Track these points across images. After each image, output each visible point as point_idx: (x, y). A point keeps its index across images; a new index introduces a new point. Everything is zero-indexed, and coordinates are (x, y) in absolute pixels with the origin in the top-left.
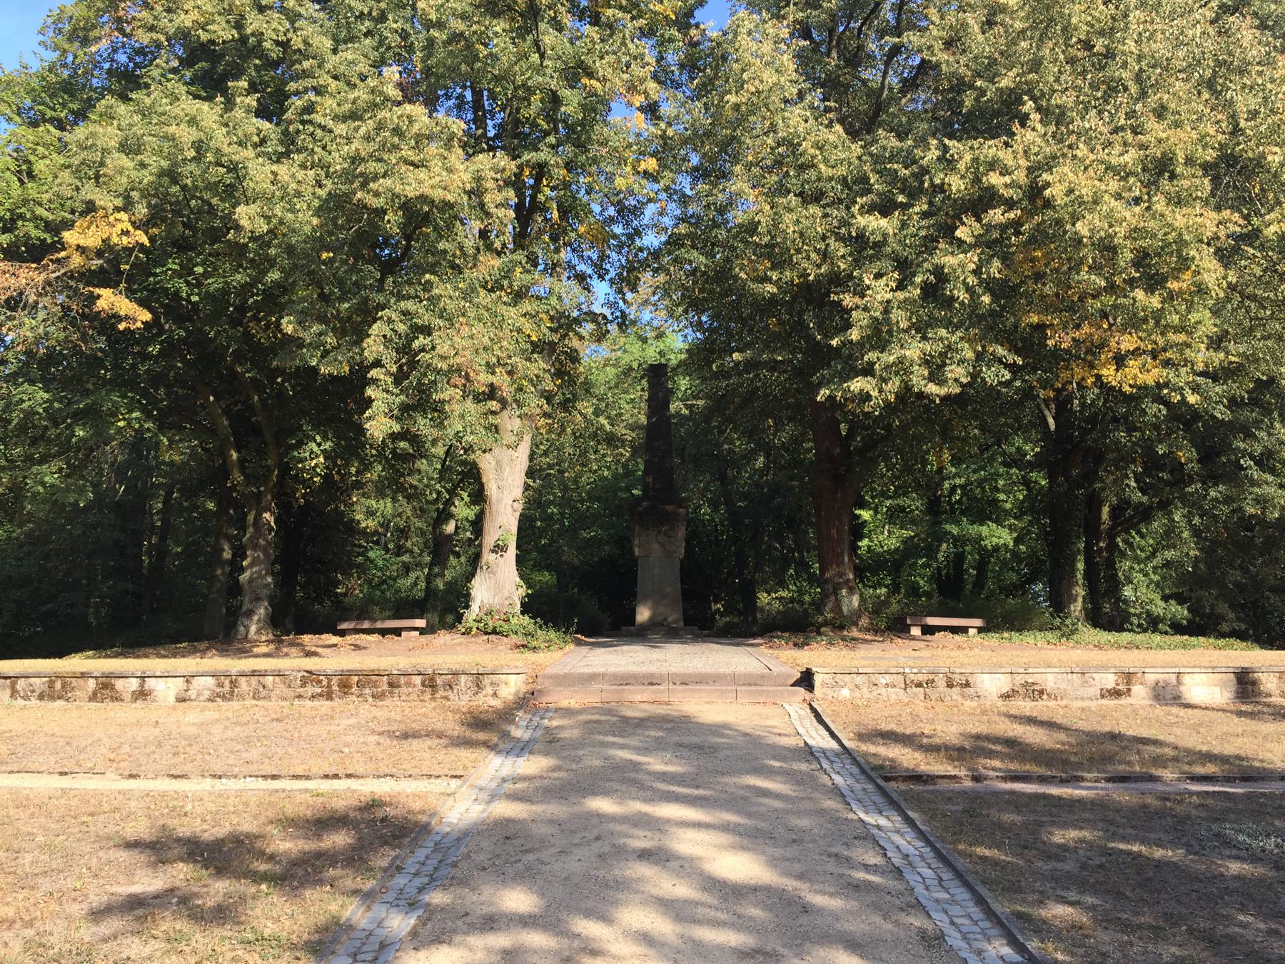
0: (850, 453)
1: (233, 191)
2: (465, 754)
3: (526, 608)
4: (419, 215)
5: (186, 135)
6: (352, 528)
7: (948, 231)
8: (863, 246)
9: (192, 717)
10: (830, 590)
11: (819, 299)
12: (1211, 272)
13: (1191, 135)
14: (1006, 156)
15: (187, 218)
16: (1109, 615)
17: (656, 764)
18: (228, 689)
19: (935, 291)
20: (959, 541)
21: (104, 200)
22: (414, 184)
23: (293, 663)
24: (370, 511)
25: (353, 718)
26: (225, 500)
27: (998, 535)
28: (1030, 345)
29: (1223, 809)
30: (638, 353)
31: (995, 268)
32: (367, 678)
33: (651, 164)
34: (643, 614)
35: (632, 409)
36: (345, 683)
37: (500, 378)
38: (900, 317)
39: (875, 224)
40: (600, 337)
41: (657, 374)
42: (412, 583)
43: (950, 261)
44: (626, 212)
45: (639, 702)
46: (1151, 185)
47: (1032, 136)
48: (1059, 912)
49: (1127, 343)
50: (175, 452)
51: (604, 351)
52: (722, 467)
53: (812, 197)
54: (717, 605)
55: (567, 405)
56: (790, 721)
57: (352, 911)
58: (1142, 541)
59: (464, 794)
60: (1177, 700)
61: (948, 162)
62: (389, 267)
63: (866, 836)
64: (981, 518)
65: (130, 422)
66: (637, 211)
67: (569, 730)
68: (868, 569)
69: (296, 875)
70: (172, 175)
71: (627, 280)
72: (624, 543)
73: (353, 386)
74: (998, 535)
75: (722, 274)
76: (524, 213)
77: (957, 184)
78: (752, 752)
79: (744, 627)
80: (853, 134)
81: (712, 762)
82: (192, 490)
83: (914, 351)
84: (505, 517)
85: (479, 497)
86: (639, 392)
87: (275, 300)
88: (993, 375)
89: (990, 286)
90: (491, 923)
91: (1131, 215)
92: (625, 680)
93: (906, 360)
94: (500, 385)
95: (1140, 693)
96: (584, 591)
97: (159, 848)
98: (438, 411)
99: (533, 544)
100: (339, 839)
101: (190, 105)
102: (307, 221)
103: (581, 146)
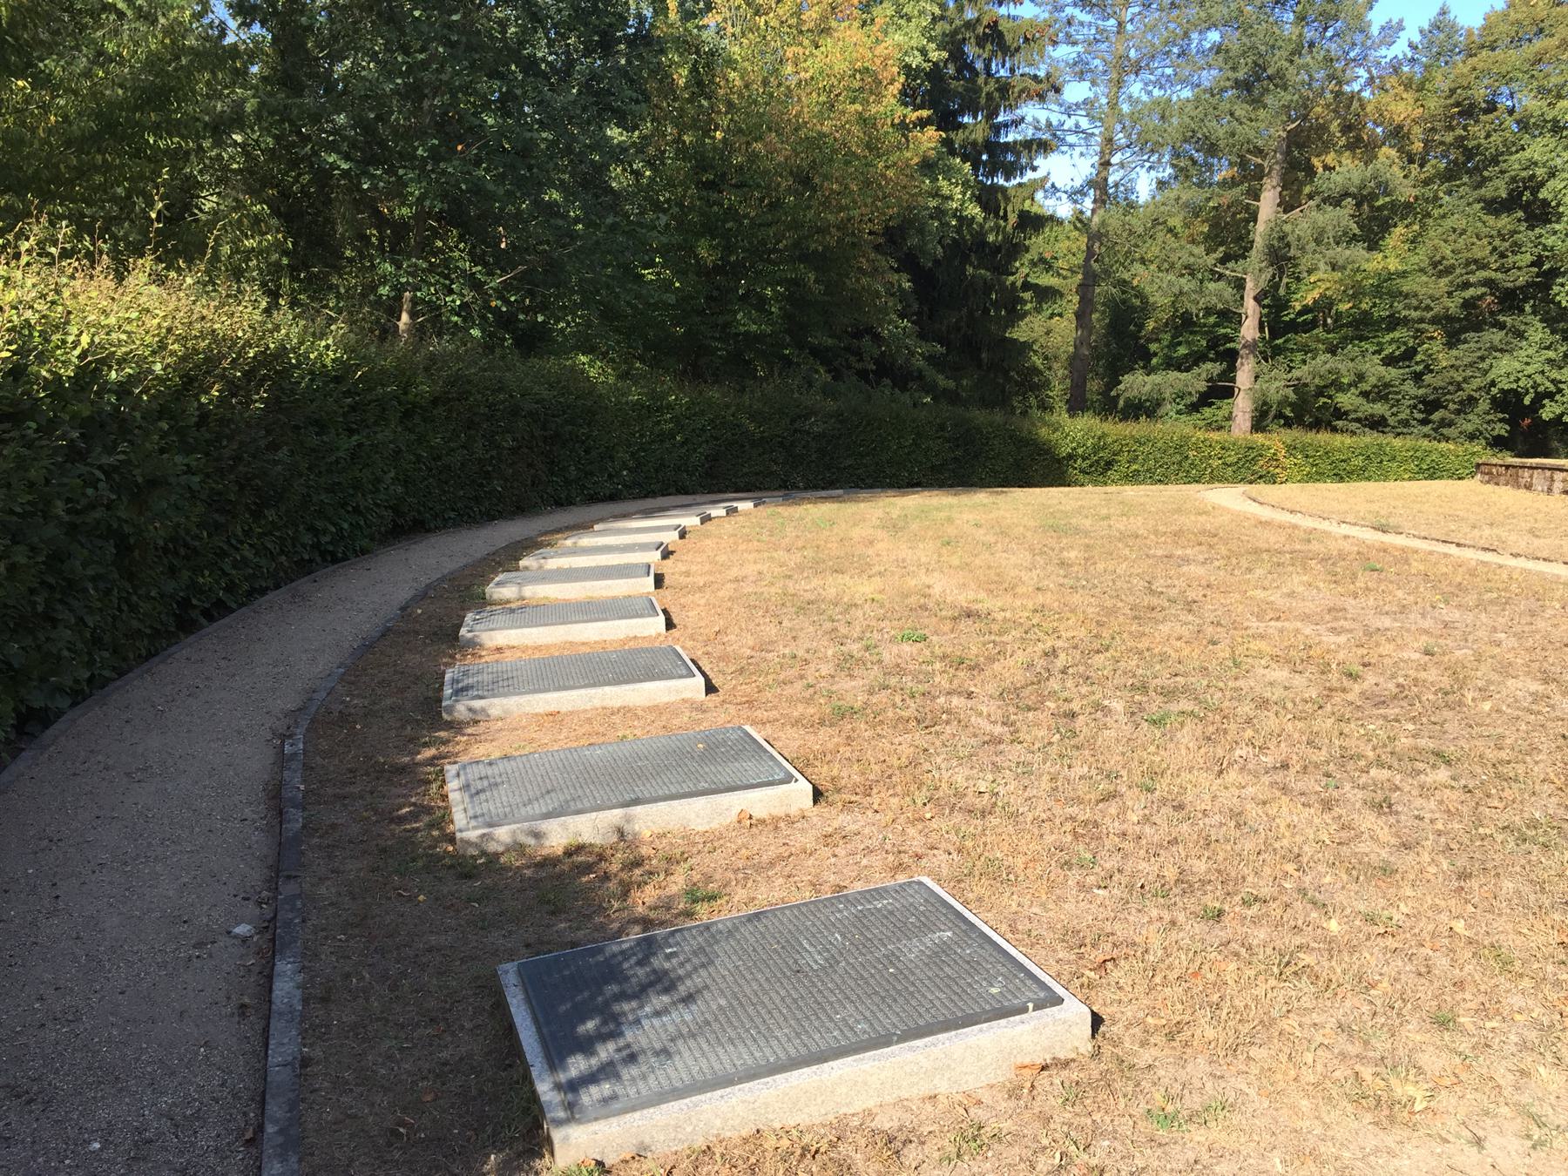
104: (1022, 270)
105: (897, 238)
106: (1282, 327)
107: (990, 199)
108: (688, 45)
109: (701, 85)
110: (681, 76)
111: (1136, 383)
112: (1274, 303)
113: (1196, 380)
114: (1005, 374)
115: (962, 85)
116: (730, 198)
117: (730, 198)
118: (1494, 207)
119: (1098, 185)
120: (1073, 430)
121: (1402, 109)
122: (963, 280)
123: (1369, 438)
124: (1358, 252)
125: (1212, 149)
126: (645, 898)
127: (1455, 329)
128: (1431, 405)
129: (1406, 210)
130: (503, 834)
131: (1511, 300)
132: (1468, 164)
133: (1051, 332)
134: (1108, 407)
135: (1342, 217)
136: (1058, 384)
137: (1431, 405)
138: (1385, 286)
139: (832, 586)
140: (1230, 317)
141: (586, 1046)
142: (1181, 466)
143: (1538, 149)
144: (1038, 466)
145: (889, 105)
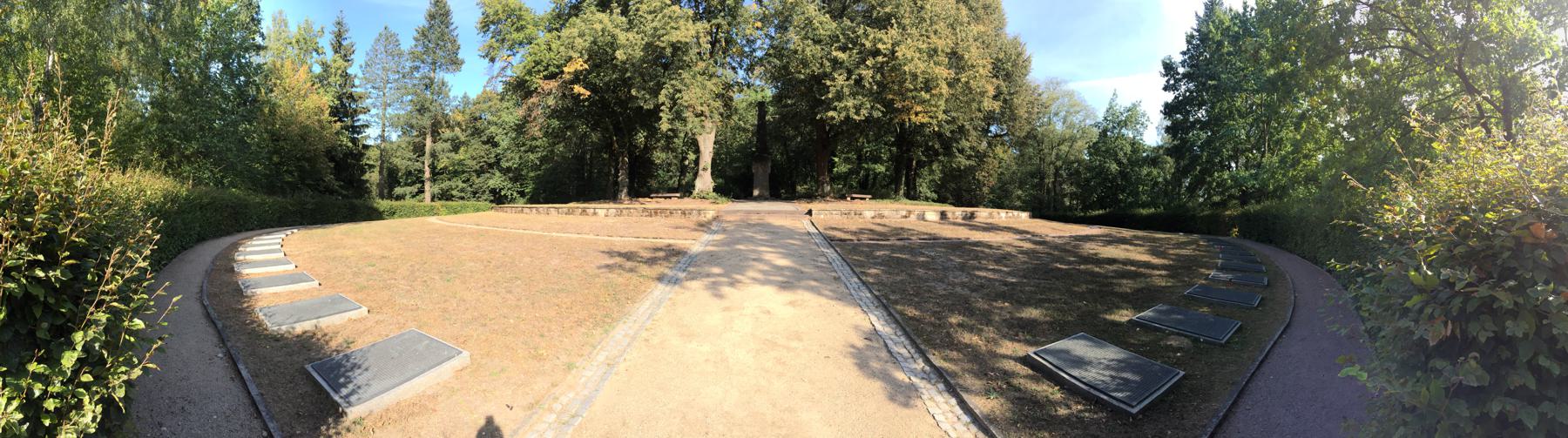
0: (828, 138)
1: (613, 45)
2: (696, 234)
3: (715, 190)
4: (677, 48)
5: (598, 27)
6: (652, 163)
7: (864, 61)
8: (836, 63)
9: (610, 221)
10: (820, 184)
11: (818, 81)
12: (945, 89)
13: (943, 44)
14: (885, 38)
15: (600, 56)
16: (912, 195)
17: (759, 237)
18: (620, 213)
19: (859, 81)
20: (867, 170)
21: (575, 55)
22: (675, 36)
23: (637, 206)
24: (659, 156)
25: (658, 221)
26: (612, 153)
27: (880, 168)
28: (889, 105)
29: (922, 246)
30: (755, 97)
31: (878, 77)
32: (663, 210)
33: (759, 24)
34: (756, 193)
35: (752, 118)
36: (656, 212)
37: (705, 109)
38: (846, 90)
39: (841, 55)
40: (741, 91)
41: (761, 105)
42: (674, 182)
43: (864, 72)
44: (750, 42)
45: (754, 219)
46: (930, 56)
47: (894, 32)
48: (873, 271)
49: (919, 109)
50: (595, 137)
51: (742, 96)
52: (785, 141)
53: (817, 42)
54: (781, 190)
55: (729, 117)
56: (804, 224)
57: (667, 271)
58: (925, 171)
59: (697, 244)
60: (923, 219)
61: (866, 35)
62: (666, 67)
63: (823, 255)
64: (875, 162)
65: (583, 128)
66: (754, 42)
67: (730, 227)
68: (834, 180)
69: (651, 261)
70: (594, 42)
71: (750, 69)
72: (749, 168)
73: (655, 113)
74: (880, 168)
75: (785, 67)
76: (713, 44)
77: (868, 45)
78: (791, 233)
79: (792, 196)
80: (834, 18)
81: (776, 236)
82: (599, 151)
83: (850, 103)
84: (707, 158)
85: (697, 151)
86: (754, 112)
87: (627, 83)
88: (877, 114)
89: (878, 83)
90: (708, 275)
91: (922, 66)
92: (749, 212)
93: (850, 107)
94: (706, 109)
95: (913, 217)
96: (734, 184)
97: (611, 254)
98: (684, 120)
99: (717, 170)
100: (661, 254)
101: (600, 15)
102: (639, 54)
103: (734, 18)
104: (365, 161)
105: (330, 154)
106: (436, 174)
107: (354, 141)
108: (269, 102)
109: (273, 112)
110: (266, 110)
111: (398, 190)
112: (433, 167)
113: (414, 189)
114: (361, 188)
115: (345, 109)
116: (282, 143)
117: (282, 143)
118: (484, 143)
119: (382, 137)
120: (383, 204)
121: (460, 118)
122: (348, 163)
123: (461, 202)
124: (453, 154)
125: (412, 127)
126: (333, 344)
127: (479, 173)
128: (475, 193)
129: (463, 143)
130: (284, 328)
131: (491, 166)
132: (477, 132)
133: (373, 177)
134: (390, 197)
135: (448, 145)
136: (375, 190)
137: (475, 193)
138: (461, 163)
139: (339, 253)
140: (421, 171)
141: (344, 385)
142: (413, 212)
143: (493, 129)
144: (374, 215)
145: (326, 116)
